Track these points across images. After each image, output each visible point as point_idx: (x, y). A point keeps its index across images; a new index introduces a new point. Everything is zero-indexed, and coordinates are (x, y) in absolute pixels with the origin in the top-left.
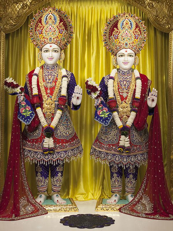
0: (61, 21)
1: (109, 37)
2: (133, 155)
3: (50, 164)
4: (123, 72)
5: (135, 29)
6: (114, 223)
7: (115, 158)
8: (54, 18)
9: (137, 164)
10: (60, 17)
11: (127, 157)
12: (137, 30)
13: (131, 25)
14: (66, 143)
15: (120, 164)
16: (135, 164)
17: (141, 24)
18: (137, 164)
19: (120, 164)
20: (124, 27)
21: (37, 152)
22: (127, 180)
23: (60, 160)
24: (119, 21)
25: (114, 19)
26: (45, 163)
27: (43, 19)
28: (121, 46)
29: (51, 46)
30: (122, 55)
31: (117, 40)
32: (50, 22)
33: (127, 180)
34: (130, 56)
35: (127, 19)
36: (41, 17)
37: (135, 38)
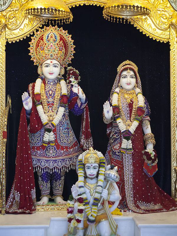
0: (61, 40)
1: (36, 48)
2: (116, 155)
3: (48, 172)
4: (49, 82)
5: (59, 42)
6: (68, 222)
7: (57, 164)
8: (55, 37)
9: (72, 166)
10: (60, 35)
11: (53, 161)
12: (61, 42)
13: (56, 38)
14: (70, 148)
15: (46, 170)
16: (71, 167)
17: (68, 37)
18: (72, 166)
19: (46, 170)
20: (49, 40)
21: (56, 160)
22: (59, 182)
23: (72, 165)
24: (44, 35)
25: (40, 33)
26: (50, 170)
27: (45, 38)
28: (46, 57)
29: (51, 62)
30: (47, 66)
31: (43, 51)
32: (51, 40)
33: (59, 182)
34: (55, 66)
35: (52, 33)
36: (43, 36)
37: (59, 50)
